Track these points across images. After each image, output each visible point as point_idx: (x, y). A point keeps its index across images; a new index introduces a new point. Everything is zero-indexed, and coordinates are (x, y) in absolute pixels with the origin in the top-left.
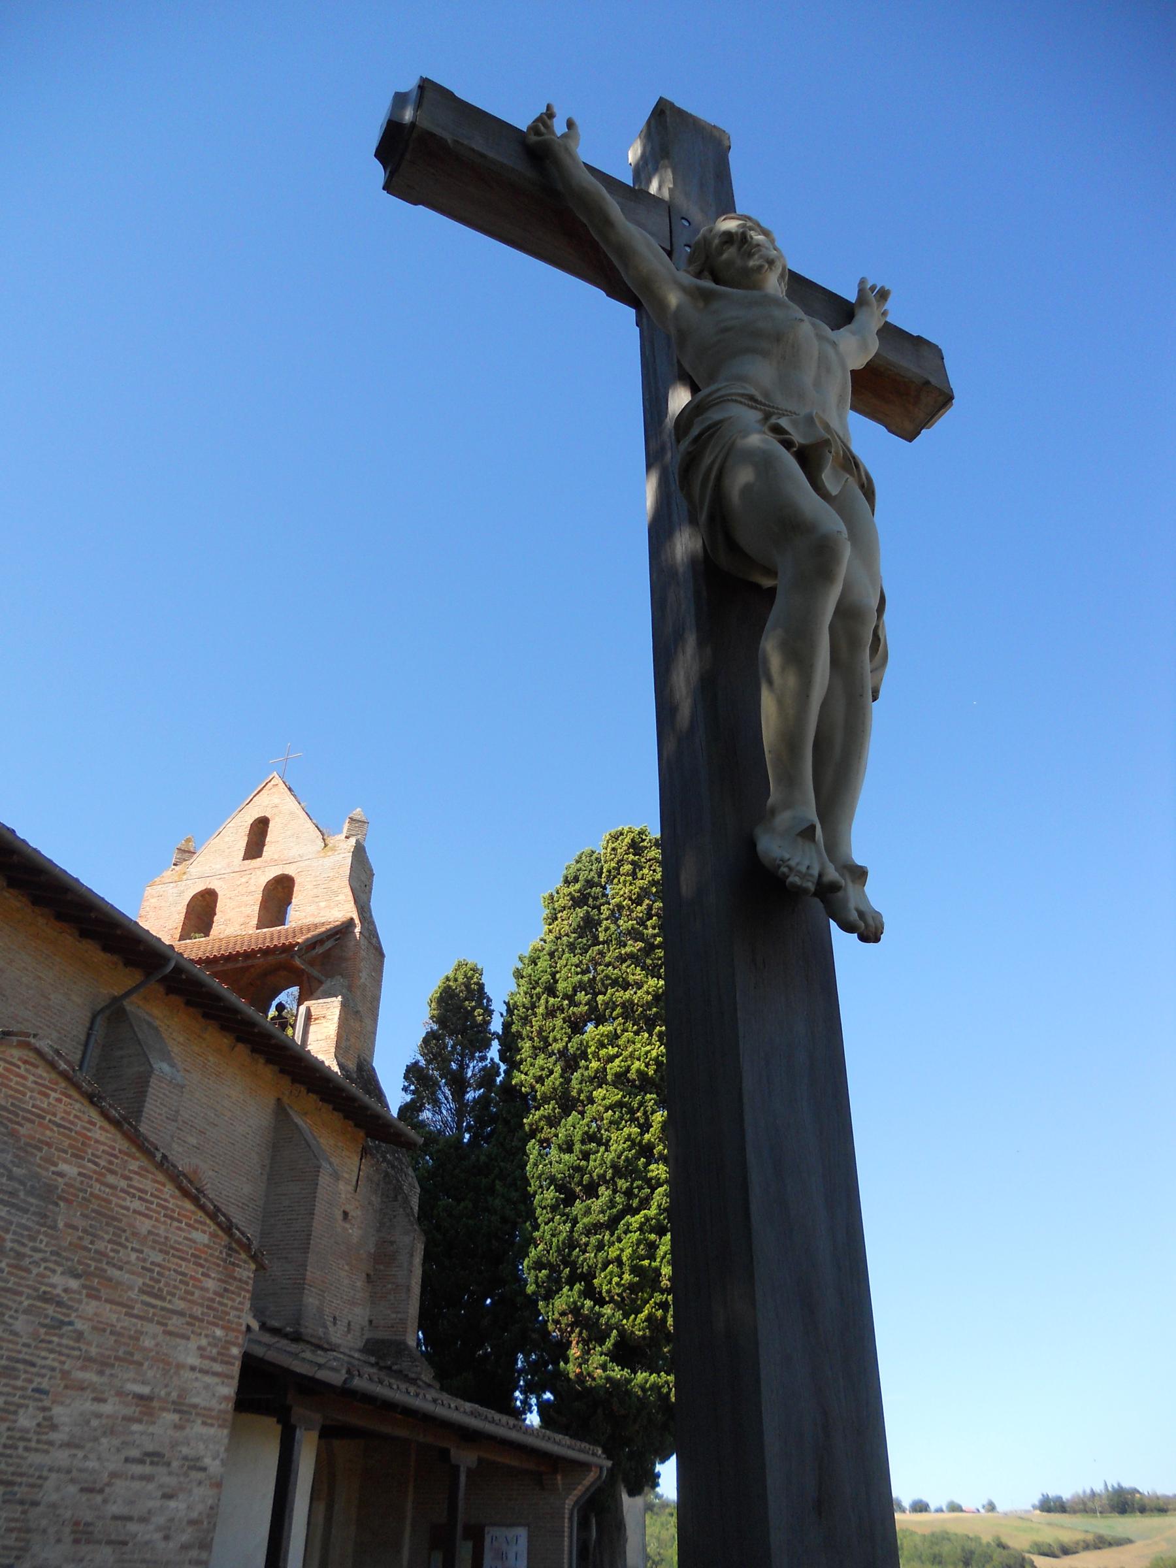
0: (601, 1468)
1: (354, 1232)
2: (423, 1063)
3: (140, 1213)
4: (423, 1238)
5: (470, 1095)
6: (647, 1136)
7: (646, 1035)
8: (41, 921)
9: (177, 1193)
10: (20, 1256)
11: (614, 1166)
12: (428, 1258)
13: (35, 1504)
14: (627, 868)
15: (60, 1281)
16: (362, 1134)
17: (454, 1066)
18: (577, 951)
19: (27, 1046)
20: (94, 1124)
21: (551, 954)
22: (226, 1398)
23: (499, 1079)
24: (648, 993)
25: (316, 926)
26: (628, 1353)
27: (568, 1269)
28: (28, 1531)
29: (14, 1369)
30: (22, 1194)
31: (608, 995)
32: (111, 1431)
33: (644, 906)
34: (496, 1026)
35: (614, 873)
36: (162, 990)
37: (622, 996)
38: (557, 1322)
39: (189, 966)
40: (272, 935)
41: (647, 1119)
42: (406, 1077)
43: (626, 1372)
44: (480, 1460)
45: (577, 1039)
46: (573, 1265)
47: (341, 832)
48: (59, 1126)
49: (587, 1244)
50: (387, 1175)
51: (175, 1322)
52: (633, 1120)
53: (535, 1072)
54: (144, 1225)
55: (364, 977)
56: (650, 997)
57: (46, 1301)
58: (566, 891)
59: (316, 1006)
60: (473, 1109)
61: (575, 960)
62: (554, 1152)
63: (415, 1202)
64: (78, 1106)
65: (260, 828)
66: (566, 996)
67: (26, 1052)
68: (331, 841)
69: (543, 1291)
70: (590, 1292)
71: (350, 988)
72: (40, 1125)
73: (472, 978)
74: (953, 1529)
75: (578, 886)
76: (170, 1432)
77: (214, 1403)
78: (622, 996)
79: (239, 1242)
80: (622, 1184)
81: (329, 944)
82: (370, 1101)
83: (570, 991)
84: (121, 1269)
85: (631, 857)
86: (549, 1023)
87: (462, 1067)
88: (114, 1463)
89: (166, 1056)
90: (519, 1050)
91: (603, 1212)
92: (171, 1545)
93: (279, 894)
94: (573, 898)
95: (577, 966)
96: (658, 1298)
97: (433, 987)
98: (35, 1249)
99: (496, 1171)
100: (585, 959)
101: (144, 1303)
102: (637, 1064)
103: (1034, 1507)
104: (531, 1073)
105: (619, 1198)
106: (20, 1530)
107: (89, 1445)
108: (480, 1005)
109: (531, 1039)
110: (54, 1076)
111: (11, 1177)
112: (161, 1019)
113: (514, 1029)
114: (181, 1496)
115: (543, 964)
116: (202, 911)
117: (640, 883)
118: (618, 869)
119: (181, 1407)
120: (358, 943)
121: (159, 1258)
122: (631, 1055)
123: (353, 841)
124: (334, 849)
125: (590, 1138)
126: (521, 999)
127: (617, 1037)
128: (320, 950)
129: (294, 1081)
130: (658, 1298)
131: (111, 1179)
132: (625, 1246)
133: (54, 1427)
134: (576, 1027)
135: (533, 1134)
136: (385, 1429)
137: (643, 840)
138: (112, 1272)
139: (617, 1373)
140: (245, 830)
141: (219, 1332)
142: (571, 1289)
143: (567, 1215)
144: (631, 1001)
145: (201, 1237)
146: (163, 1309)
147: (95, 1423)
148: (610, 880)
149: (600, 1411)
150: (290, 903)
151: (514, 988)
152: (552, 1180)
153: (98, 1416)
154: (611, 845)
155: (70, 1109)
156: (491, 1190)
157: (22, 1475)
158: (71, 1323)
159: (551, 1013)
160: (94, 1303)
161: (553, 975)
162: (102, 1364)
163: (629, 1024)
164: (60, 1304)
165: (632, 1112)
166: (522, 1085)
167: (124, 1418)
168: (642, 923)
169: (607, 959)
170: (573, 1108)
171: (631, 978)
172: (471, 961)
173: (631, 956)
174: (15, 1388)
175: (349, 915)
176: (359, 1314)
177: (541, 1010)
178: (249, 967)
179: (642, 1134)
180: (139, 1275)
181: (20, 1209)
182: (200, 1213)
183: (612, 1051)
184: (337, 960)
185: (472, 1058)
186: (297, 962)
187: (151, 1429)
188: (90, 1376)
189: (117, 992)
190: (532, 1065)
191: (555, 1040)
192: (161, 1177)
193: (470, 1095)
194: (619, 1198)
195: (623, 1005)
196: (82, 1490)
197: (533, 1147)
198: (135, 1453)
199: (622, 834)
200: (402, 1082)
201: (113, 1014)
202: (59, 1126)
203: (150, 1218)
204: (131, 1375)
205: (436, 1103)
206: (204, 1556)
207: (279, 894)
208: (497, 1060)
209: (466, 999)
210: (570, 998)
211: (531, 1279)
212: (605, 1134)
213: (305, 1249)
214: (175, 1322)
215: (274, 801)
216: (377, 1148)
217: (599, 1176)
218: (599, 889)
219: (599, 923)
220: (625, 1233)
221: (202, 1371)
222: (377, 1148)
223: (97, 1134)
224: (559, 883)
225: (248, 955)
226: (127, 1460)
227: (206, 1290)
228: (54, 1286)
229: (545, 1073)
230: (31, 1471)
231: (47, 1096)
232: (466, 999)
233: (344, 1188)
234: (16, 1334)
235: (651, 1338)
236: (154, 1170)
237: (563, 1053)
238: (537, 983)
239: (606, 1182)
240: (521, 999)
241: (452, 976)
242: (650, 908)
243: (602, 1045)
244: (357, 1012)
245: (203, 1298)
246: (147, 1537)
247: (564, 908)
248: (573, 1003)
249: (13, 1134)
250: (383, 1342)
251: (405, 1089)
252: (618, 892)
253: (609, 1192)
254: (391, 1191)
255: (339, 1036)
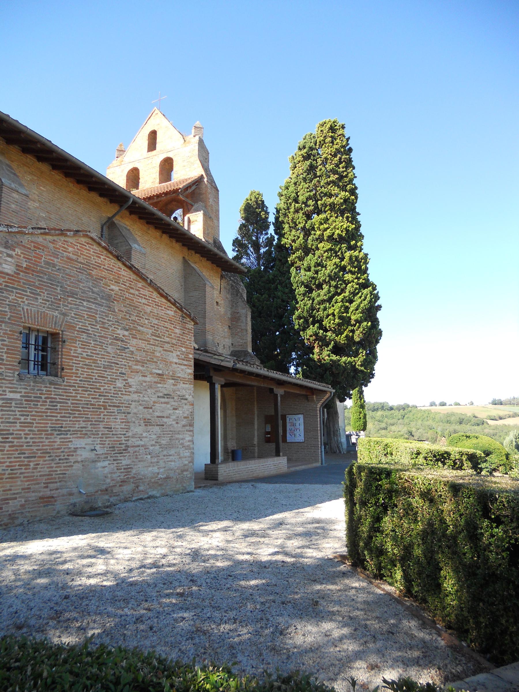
0: (331, 393)
1: (222, 310)
2: (240, 238)
3: (146, 304)
4: (250, 310)
5: (262, 250)
6: (343, 263)
7: (341, 218)
8: (71, 185)
9: (159, 296)
10: (103, 323)
11: (329, 276)
12: (252, 318)
13: (129, 413)
14: (329, 139)
15: (121, 332)
16: (220, 270)
17: (254, 238)
18: (307, 181)
19: (87, 236)
20: (121, 269)
21: (295, 184)
22: (190, 374)
23: (274, 243)
24: (341, 198)
25: (186, 180)
26: (338, 350)
27: (311, 318)
28: (128, 422)
29: (111, 366)
30: (99, 299)
31: (323, 201)
32: (150, 387)
33: (338, 158)
34: (271, 219)
35: (322, 142)
36: (127, 213)
37: (330, 201)
38: (308, 339)
39: (139, 200)
40: (166, 187)
41: (343, 255)
42: (233, 245)
43: (338, 357)
44: (285, 391)
45: (309, 222)
46: (314, 317)
47: (191, 134)
48: (107, 270)
49: (319, 309)
50: (232, 286)
51: (167, 346)
52: (337, 256)
53: (291, 237)
54: (148, 309)
55: (211, 201)
56: (342, 201)
57: (117, 340)
58: (300, 153)
59: (192, 216)
60: (263, 256)
61: (307, 186)
62: (302, 271)
63: (245, 296)
64: (113, 261)
65: (153, 136)
66: (303, 203)
67: (87, 239)
68: (187, 139)
69: (301, 328)
70: (321, 327)
71: (206, 207)
72: (100, 270)
73: (258, 198)
74: (455, 411)
75: (305, 150)
76: (172, 387)
77: (186, 376)
78: (330, 201)
79: (186, 314)
80: (333, 283)
81: (194, 188)
82: (221, 254)
83: (305, 200)
84: (142, 327)
85: (330, 134)
86: (296, 215)
87: (257, 238)
88: (154, 398)
89: (136, 241)
90: (283, 228)
91: (325, 295)
92: (179, 425)
93: (167, 167)
94: (303, 157)
95: (307, 188)
96: (350, 328)
97: (241, 204)
98: (108, 320)
99: (278, 281)
100: (311, 185)
101: (153, 339)
102: (337, 232)
103: (489, 403)
104: (289, 238)
105: (332, 289)
106: (125, 422)
107: (144, 392)
108: (263, 210)
109: (289, 223)
110: (101, 249)
111: (93, 292)
112: (129, 225)
113: (280, 219)
114: (180, 409)
115: (291, 189)
116: (134, 176)
117: (335, 146)
118: (324, 141)
119: (173, 378)
120: (206, 186)
121: (156, 322)
122: (335, 228)
123: (197, 138)
124: (189, 142)
125: (318, 265)
126: (282, 206)
127: (328, 220)
128: (190, 191)
129: (189, 249)
130: (350, 328)
131: (132, 291)
132: (336, 308)
133: (130, 386)
134: (309, 216)
135: (292, 264)
136: (249, 383)
137: (336, 126)
138: (139, 328)
139: (334, 357)
140: (146, 137)
141: (184, 349)
142: (314, 326)
143: (310, 297)
144: (333, 203)
145: (171, 313)
146: (161, 341)
147: (144, 384)
148: (321, 146)
149: (328, 372)
150: (172, 170)
151: (279, 202)
152: (303, 283)
153: (145, 382)
154: (320, 129)
155: (110, 262)
156: (276, 288)
157: (122, 403)
158: (128, 348)
159: (297, 211)
160: (135, 340)
161: (297, 193)
162: (143, 363)
163: (333, 213)
164: (122, 341)
165: (336, 252)
166: (286, 244)
167: (155, 382)
168: (337, 166)
169: (322, 184)
170: (309, 252)
171: (333, 192)
172: (257, 191)
173: (333, 182)
174: (113, 373)
175: (200, 174)
176: (228, 342)
177: (292, 210)
178: (159, 202)
179: (341, 262)
180: (150, 329)
181: (99, 305)
182: (169, 303)
183: (326, 226)
184: (197, 194)
185: (262, 234)
186: (181, 197)
187: (165, 386)
188: (139, 367)
189: (110, 215)
190: (290, 235)
191: (299, 223)
192: (151, 290)
193: (262, 250)
194: (332, 289)
195: (330, 205)
196: (144, 408)
197: (293, 270)
198: (161, 394)
199: (325, 123)
200: (232, 247)
201: (109, 226)
202: (107, 270)
203: (150, 306)
204: (154, 367)
205: (248, 255)
206: (191, 429)
207: (167, 167)
208: (273, 234)
209: (256, 208)
210: (305, 203)
211: (297, 323)
212: (325, 263)
213: (204, 317)
214: (167, 346)
215: (158, 122)
216: (227, 275)
217: (323, 281)
218: (316, 151)
219: (317, 167)
220: (336, 303)
221: (179, 364)
222: (227, 275)
223: (123, 273)
224: (297, 150)
225: (158, 196)
226: (158, 397)
227: (176, 333)
228: (119, 334)
229: (296, 238)
230: (125, 402)
231: (100, 258)
232: (256, 208)
233: (216, 293)
234: (109, 353)
235: (347, 344)
236: (147, 286)
237: (304, 228)
238: (289, 197)
239: (326, 283)
240: (282, 206)
241: (249, 198)
242: (340, 159)
243: (321, 224)
244: (210, 217)
245: (175, 336)
246: (170, 423)
247: (299, 161)
248: (307, 206)
249: (90, 274)
250: (238, 351)
251: (234, 250)
252: (324, 152)
253: (328, 287)
254: (234, 292)
255: (204, 228)
